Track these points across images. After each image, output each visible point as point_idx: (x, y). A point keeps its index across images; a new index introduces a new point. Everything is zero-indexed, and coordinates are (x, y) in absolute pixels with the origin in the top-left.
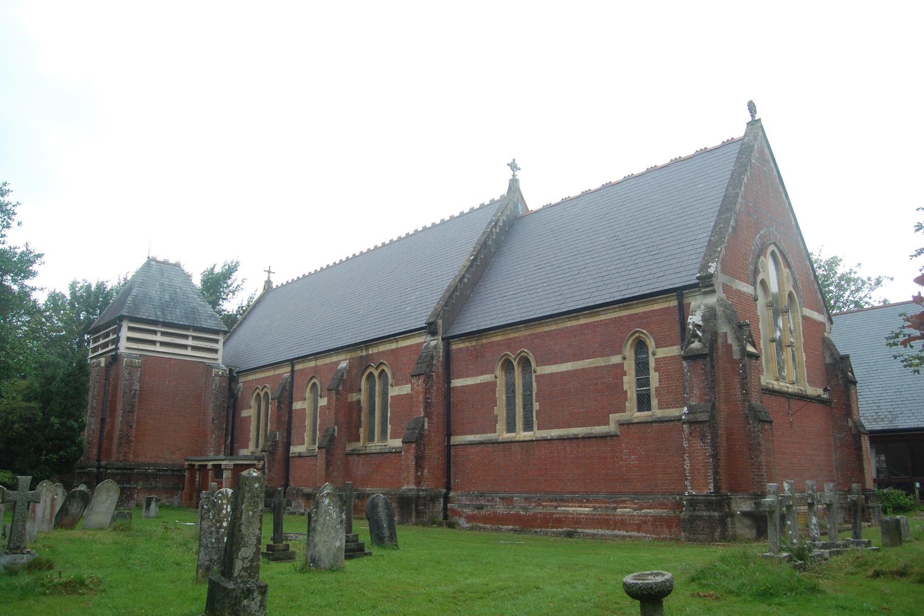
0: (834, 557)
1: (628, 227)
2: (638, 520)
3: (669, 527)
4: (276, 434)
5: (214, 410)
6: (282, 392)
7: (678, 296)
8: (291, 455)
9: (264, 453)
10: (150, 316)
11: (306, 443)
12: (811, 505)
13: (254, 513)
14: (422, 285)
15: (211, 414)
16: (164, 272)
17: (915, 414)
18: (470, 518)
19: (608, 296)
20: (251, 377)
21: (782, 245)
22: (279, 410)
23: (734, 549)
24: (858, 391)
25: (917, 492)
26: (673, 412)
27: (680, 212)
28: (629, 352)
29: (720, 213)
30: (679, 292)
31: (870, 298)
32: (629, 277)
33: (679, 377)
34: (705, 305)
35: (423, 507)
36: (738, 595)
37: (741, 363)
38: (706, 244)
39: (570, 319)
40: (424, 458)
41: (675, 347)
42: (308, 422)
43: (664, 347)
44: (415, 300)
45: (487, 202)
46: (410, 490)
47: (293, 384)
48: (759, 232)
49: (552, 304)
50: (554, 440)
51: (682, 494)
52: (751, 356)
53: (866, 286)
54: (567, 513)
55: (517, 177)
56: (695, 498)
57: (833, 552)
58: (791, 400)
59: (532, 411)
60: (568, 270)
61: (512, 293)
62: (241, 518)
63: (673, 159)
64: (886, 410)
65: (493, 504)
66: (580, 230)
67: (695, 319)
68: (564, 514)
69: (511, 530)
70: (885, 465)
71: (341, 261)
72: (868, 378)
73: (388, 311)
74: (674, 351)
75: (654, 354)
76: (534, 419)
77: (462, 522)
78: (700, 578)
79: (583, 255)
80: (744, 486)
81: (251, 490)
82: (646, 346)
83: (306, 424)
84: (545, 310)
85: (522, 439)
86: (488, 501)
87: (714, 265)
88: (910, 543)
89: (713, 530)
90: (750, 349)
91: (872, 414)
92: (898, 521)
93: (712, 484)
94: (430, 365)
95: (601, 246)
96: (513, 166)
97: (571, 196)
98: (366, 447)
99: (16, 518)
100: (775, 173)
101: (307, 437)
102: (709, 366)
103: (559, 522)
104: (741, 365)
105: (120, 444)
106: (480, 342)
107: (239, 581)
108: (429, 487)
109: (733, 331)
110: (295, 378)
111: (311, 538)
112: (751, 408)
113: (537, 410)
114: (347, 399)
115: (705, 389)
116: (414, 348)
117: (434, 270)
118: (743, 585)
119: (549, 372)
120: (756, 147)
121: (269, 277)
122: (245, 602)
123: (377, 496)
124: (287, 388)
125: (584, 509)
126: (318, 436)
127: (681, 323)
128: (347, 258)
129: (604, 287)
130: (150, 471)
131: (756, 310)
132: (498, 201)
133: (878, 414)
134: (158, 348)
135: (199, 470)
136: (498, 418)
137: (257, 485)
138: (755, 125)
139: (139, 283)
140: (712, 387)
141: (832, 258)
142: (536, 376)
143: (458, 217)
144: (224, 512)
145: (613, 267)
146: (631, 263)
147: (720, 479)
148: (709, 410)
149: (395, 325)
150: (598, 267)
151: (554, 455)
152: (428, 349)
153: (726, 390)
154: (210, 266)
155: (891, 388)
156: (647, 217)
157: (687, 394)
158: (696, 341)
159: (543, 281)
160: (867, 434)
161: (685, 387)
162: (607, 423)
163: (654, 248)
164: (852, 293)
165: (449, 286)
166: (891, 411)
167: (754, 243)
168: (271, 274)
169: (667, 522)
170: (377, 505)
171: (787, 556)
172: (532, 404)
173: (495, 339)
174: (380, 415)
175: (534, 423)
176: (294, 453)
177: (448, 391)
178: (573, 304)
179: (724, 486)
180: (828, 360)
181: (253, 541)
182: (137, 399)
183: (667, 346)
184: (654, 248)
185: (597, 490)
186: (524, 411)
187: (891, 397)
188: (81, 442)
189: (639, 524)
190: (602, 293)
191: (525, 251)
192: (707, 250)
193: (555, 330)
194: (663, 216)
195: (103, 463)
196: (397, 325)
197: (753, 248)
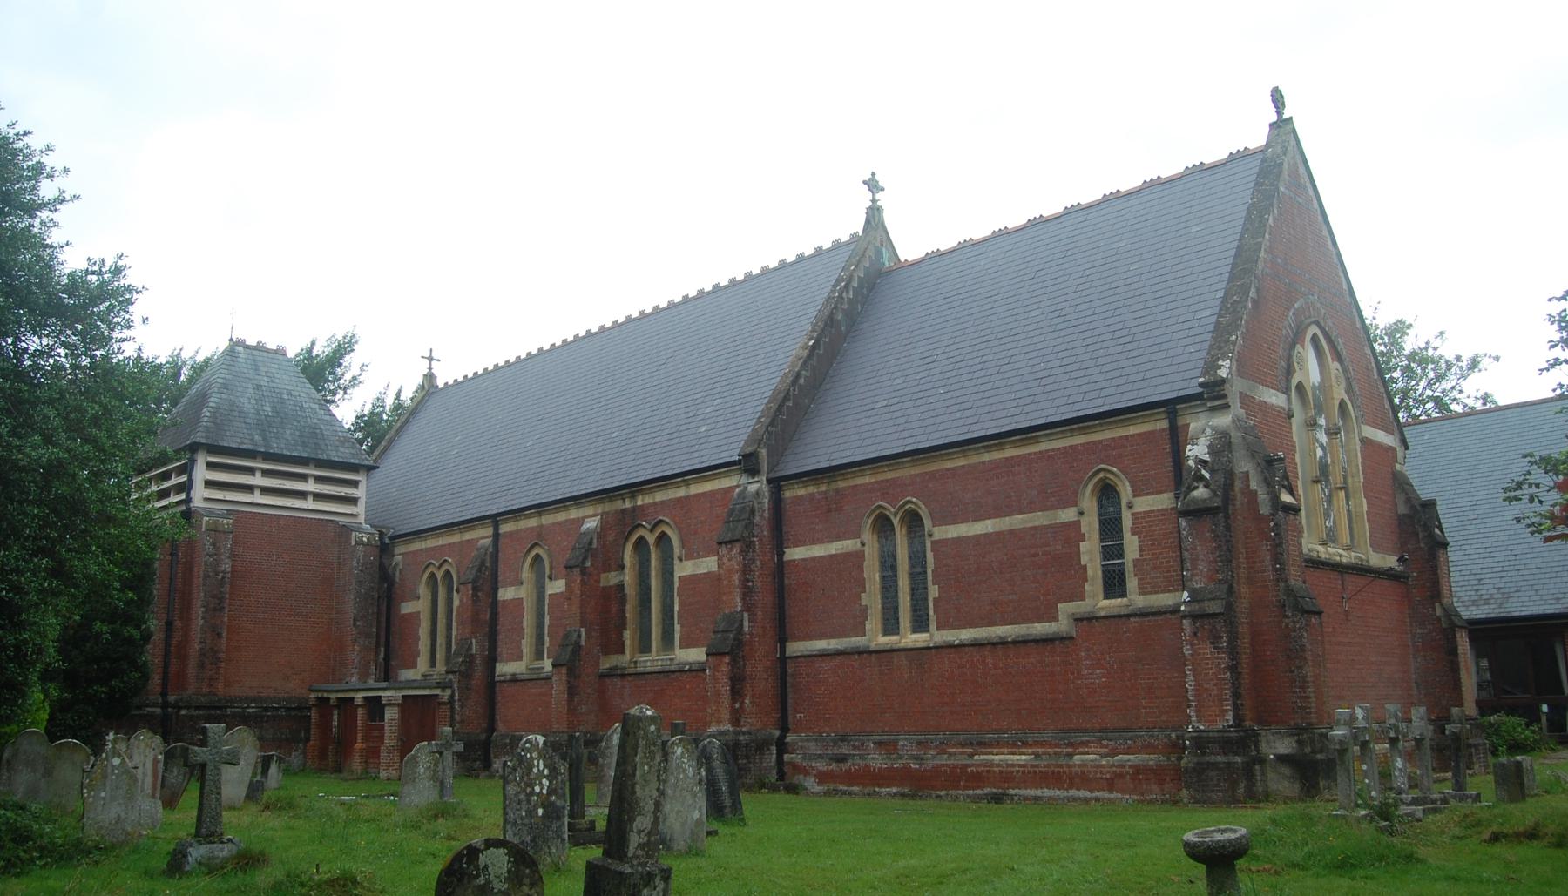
0: (1431, 817)
2: (1108, 772)
3: (1161, 782)
4: (471, 643)
6: (479, 570)
7: (1169, 413)
8: (497, 678)
10: (243, 443)
11: (524, 658)
13: (650, 767)
14: (724, 389)
15: (351, 609)
16: (260, 364)
17: (1540, 593)
18: (822, 777)
19: (1051, 412)
23: (1266, 812)
25: (1544, 719)
26: (1165, 600)
28: (1089, 502)
29: (1233, 277)
30: (1171, 407)
31: (1461, 392)
32: (1086, 380)
33: (1173, 542)
34: (1213, 428)
36: (1304, 869)
37: (1272, 520)
38: (1211, 327)
39: (988, 449)
40: (744, 679)
41: (1165, 495)
42: (528, 622)
43: (1147, 494)
45: (827, 245)
49: (956, 423)
50: (964, 645)
51: (1179, 729)
53: (1453, 370)
54: (991, 764)
55: (879, 203)
56: (1205, 734)
57: (1429, 809)
58: (1346, 577)
59: (926, 599)
61: (885, 403)
62: (634, 775)
63: (1148, 180)
64: (1492, 586)
65: (862, 752)
66: (994, 299)
67: (1197, 450)
69: (895, 794)
70: (1488, 676)
71: (564, 341)
72: (1462, 533)
73: (667, 432)
74: (1163, 501)
75: (1130, 506)
76: (931, 612)
77: (810, 783)
79: (1002, 341)
81: (646, 734)
82: (1116, 491)
84: (945, 433)
85: (910, 645)
86: (855, 748)
87: (1227, 363)
88: (1536, 798)
90: (1286, 498)
91: (1468, 593)
92: (1519, 763)
93: (1231, 713)
94: (750, 525)
95: (1034, 326)
96: (873, 185)
98: (636, 662)
99: (207, 789)
100: (1316, 205)
101: (527, 647)
103: (977, 779)
104: (1272, 524)
105: (202, 666)
106: (834, 486)
107: (635, 862)
108: (753, 728)
109: (1259, 469)
110: (500, 545)
112: (1290, 592)
114: (598, 581)
115: (1216, 562)
116: (719, 497)
117: (743, 362)
119: (955, 535)
120: (1286, 166)
121: (430, 369)
123: (709, 742)
124: (488, 564)
125: (1018, 757)
126: (547, 645)
128: (540, 350)
129: (1044, 397)
130: (250, 710)
132: (848, 243)
133: (1479, 593)
134: (258, 498)
135: (338, 707)
136: (869, 612)
137: (653, 728)
138: (1282, 128)
139: (219, 385)
140: (1227, 557)
141: (1395, 324)
143: (775, 269)
144: (535, 770)
145: (1057, 363)
146: (1087, 356)
147: (1242, 705)
149: (683, 457)
150: (1031, 362)
151: (965, 670)
152: (744, 498)
153: (1247, 563)
155: (1499, 549)
156: (1110, 280)
158: (1201, 485)
159: (937, 385)
162: (1055, 619)
163: (1125, 332)
164: (1430, 384)
165: (774, 390)
166: (1500, 588)
168: (434, 363)
169: (1139, 774)
171: (1367, 815)
172: (926, 588)
173: (861, 481)
175: (931, 618)
177: (780, 568)
178: (993, 423)
180: (1402, 509)
181: (650, 806)
182: (227, 588)
183: (1152, 494)
184: (1125, 332)
186: (912, 599)
187: (1501, 564)
188: (145, 663)
189: (1112, 779)
190: (1042, 406)
191: (901, 331)
193: (963, 466)
194: (1137, 279)
195: (172, 698)
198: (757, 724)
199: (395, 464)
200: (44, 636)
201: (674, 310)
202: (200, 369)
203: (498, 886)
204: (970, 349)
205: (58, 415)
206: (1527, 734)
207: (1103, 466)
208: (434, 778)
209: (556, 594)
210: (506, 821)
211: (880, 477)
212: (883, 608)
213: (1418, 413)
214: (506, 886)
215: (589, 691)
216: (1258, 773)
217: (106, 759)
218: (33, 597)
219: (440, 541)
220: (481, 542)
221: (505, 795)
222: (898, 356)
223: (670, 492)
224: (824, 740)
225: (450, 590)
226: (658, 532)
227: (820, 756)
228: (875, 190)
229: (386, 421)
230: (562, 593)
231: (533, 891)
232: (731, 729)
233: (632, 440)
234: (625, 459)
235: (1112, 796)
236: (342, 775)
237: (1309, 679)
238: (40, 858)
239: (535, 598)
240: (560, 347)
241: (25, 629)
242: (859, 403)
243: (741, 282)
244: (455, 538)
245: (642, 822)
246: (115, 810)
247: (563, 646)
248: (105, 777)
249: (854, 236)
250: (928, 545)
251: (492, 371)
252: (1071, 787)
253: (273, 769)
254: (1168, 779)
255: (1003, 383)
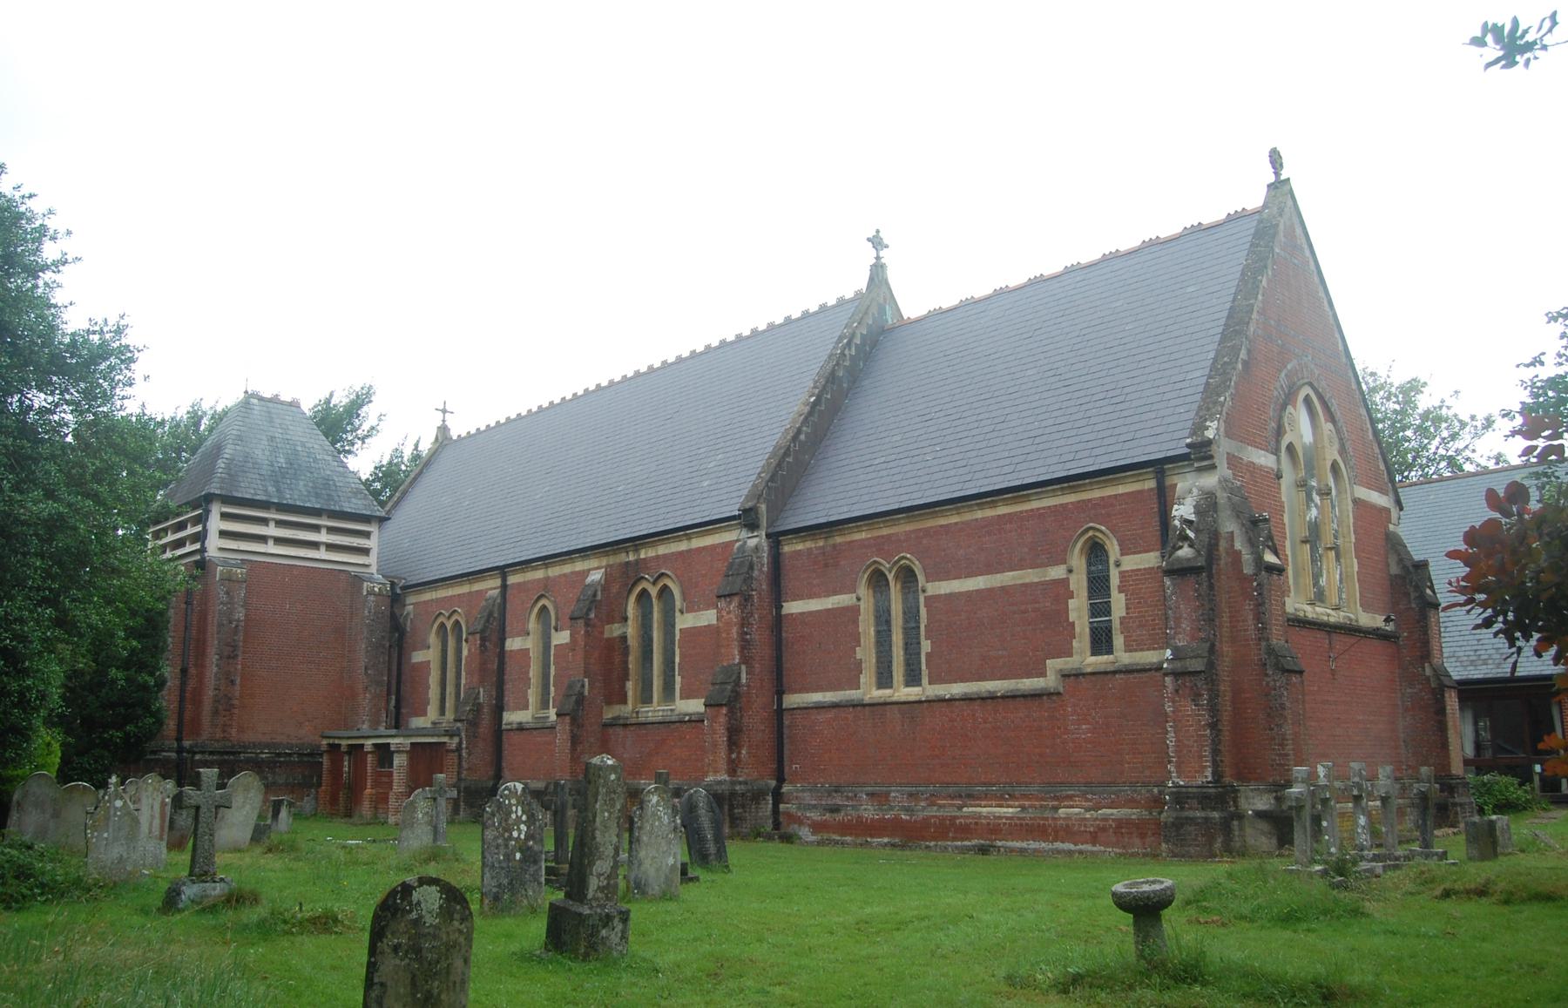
1: (1073, 354)
3: (1142, 836)
4: (479, 692)
5: (367, 652)
6: (488, 621)
8: (504, 727)
9: (459, 724)
12: (1357, 799)
13: (610, 813)
14: (728, 443)
15: (362, 660)
16: (274, 416)
18: (817, 827)
19: (1043, 470)
20: (428, 596)
21: (1322, 385)
22: (482, 652)
24: (1441, 620)
25: (1537, 779)
26: (1149, 657)
27: (1159, 331)
28: (1078, 560)
29: (1224, 337)
30: (1159, 467)
31: (1474, 451)
32: (1078, 439)
33: (1159, 600)
34: (1200, 489)
35: (740, 811)
36: (1252, 921)
37: (1255, 580)
38: (1201, 389)
39: (981, 506)
40: (741, 731)
41: (1152, 554)
42: (534, 672)
43: (1135, 553)
44: (716, 469)
45: (832, 302)
46: (720, 783)
47: (505, 608)
48: (1285, 367)
49: (951, 481)
50: (955, 700)
51: (1162, 784)
52: (1271, 568)
53: (1467, 429)
54: (980, 816)
56: (1184, 790)
57: (1389, 865)
58: (1334, 636)
59: (919, 654)
60: (976, 425)
61: (883, 459)
62: (594, 821)
64: (1491, 646)
67: (1183, 510)
68: (973, 818)
69: (886, 845)
71: (488, 426)
73: (670, 486)
75: (1118, 565)
76: (924, 667)
77: (805, 833)
78: (1198, 901)
79: (999, 399)
80: (1258, 771)
82: (1105, 551)
83: (531, 675)
84: (939, 491)
85: (903, 699)
86: (848, 798)
87: (1214, 425)
89: (1211, 840)
90: (1270, 558)
91: (1467, 653)
93: (1210, 769)
94: (748, 579)
96: (877, 242)
97: (976, 296)
98: (637, 712)
101: (533, 696)
102: (1205, 584)
103: (965, 831)
104: (1255, 584)
105: (216, 712)
106: (831, 541)
111: (634, 853)
112: (1271, 651)
113: (927, 653)
114: (602, 633)
118: (1260, 907)
119: (948, 591)
120: (1281, 227)
121: (444, 421)
122: (604, 932)
123: (695, 792)
125: (1005, 810)
126: (552, 694)
127: (1161, 517)
128: (586, 390)
130: (264, 756)
131: (1279, 493)
132: (851, 300)
133: (1478, 653)
134: (271, 548)
135: (349, 753)
136: (863, 665)
138: (1280, 189)
140: (1210, 617)
141: (1409, 382)
142: (925, 597)
143: (781, 325)
144: (514, 816)
145: (1051, 422)
146: (1080, 415)
147: (1222, 761)
148: (1206, 654)
149: (685, 512)
151: (955, 724)
152: (744, 552)
153: (1230, 622)
154: (324, 395)
157: (1171, 628)
158: (1186, 545)
159: (934, 442)
160: (1454, 688)
161: (1167, 618)
162: (1043, 674)
163: (1118, 392)
165: (775, 447)
167: (1278, 385)
168: (447, 414)
169: (1138, 828)
170: (696, 806)
172: (919, 643)
173: (857, 537)
174: (661, 660)
176: (510, 724)
177: (778, 622)
178: (986, 481)
179: (1228, 771)
180: (1395, 569)
181: (610, 851)
182: (241, 636)
183: (1139, 552)
184: (1118, 392)
185: (1027, 780)
186: (906, 654)
188: (159, 710)
189: (1096, 833)
192: (1203, 399)
193: (956, 524)
195: (187, 743)
196: (689, 510)
197: (1276, 393)
198: (754, 774)
199: (409, 515)
200: (47, 683)
201: (600, 393)
202: (218, 418)
203: (429, 920)
204: (967, 407)
205: (60, 471)
206: (1518, 793)
207: (1091, 524)
208: (430, 823)
209: (561, 645)
210: (484, 865)
211: (876, 533)
212: (878, 662)
213: (1431, 472)
214: (437, 920)
215: (592, 740)
216: (1236, 828)
217: (109, 801)
218: (36, 645)
219: (450, 592)
220: (490, 592)
221: (483, 840)
222: (898, 413)
223: (724, 534)
224: (818, 791)
225: (459, 640)
226: (660, 585)
227: (815, 807)
228: (879, 247)
229: (404, 472)
230: (567, 644)
231: (463, 926)
232: (728, 779)
233: (637, 494)
234: (629, 513)
235: (1095, 849)
236: (352, 820)
237: (1288, 737)
238: (42, 894)
239: (541, 649)
240: (570, 400)
241: (28, 676)
242: (857, 459)
243: (748, 337)
244: (464, 589)
245: (602, 866)
246: (116, 851)
247: (568, 696)
248: (107, 818)
249: (858, 294)
250: (922, 600)
251: (504, 424)
252: (1055, 840)
253: (284, 813)
254: (1150, 833)
255: (998, 441)
